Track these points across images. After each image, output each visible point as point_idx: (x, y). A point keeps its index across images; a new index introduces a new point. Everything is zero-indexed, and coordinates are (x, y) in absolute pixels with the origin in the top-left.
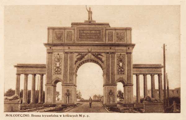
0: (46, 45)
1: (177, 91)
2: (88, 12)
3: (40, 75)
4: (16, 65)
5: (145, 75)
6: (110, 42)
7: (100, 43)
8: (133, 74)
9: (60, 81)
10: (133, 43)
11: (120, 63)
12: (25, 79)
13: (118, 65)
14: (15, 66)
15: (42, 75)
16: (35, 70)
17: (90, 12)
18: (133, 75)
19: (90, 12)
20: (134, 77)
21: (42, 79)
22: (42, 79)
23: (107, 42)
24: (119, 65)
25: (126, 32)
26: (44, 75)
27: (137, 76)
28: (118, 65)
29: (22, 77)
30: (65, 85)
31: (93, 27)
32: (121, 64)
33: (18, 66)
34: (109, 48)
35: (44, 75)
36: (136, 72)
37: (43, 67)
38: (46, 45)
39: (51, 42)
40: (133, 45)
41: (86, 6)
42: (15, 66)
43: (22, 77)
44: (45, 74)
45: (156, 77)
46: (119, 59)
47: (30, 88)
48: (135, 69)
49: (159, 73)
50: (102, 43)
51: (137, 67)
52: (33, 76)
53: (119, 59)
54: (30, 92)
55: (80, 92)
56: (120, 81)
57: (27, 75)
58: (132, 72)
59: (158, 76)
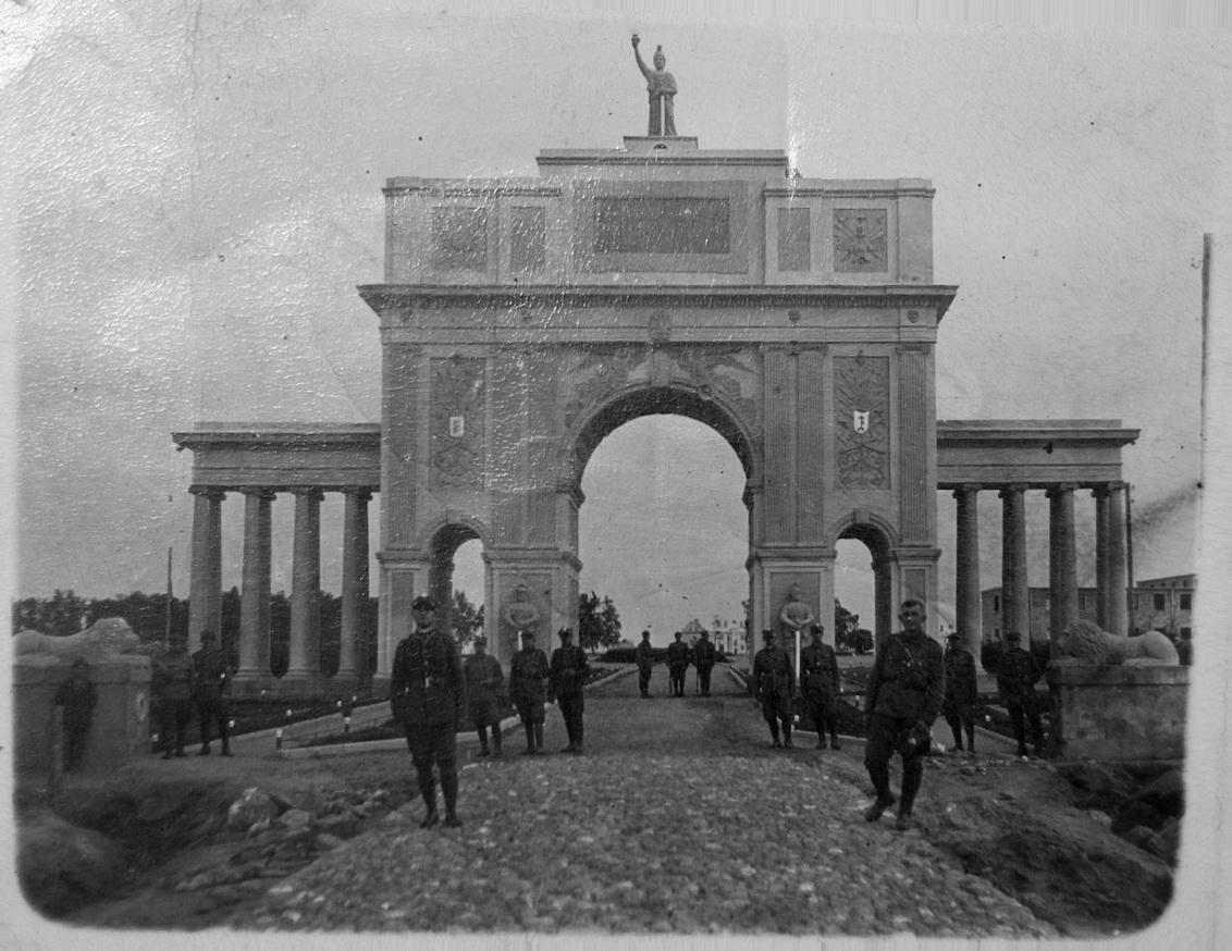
0: (375, 297)
1: (1185, 584)
2: (644, 83)
5: (263, 497)
7: (728, 280)
8: (942, 486)
9: (477, 537)
11: (857, 414)
12: (971, 447)
13: (844, 424)
14: (184, 441)
15: (361, 497)
16: (313, 467)
17: (660, 91)
18: (941, 492)
19: (660, 91)
23: (776, 277)
24: (845, 425)
27: (963, 495)
28: (844, 424)
30: (441, 764)
31: (600, 336)
32: (861, 421)
33: (209, 445)
34: (783, 316)
36: (952, 477)
37: (365, 442)
38: (375, 297)
39: (412, 273)
41: (635, 41)
42: (184, 441)
43: (234, 507)
44: (377, 489)
47: (281, 579)
48: (951, 455)
50: (738, 280)
51: (956, 438)
58: (932, 479)
59: (954, 496)
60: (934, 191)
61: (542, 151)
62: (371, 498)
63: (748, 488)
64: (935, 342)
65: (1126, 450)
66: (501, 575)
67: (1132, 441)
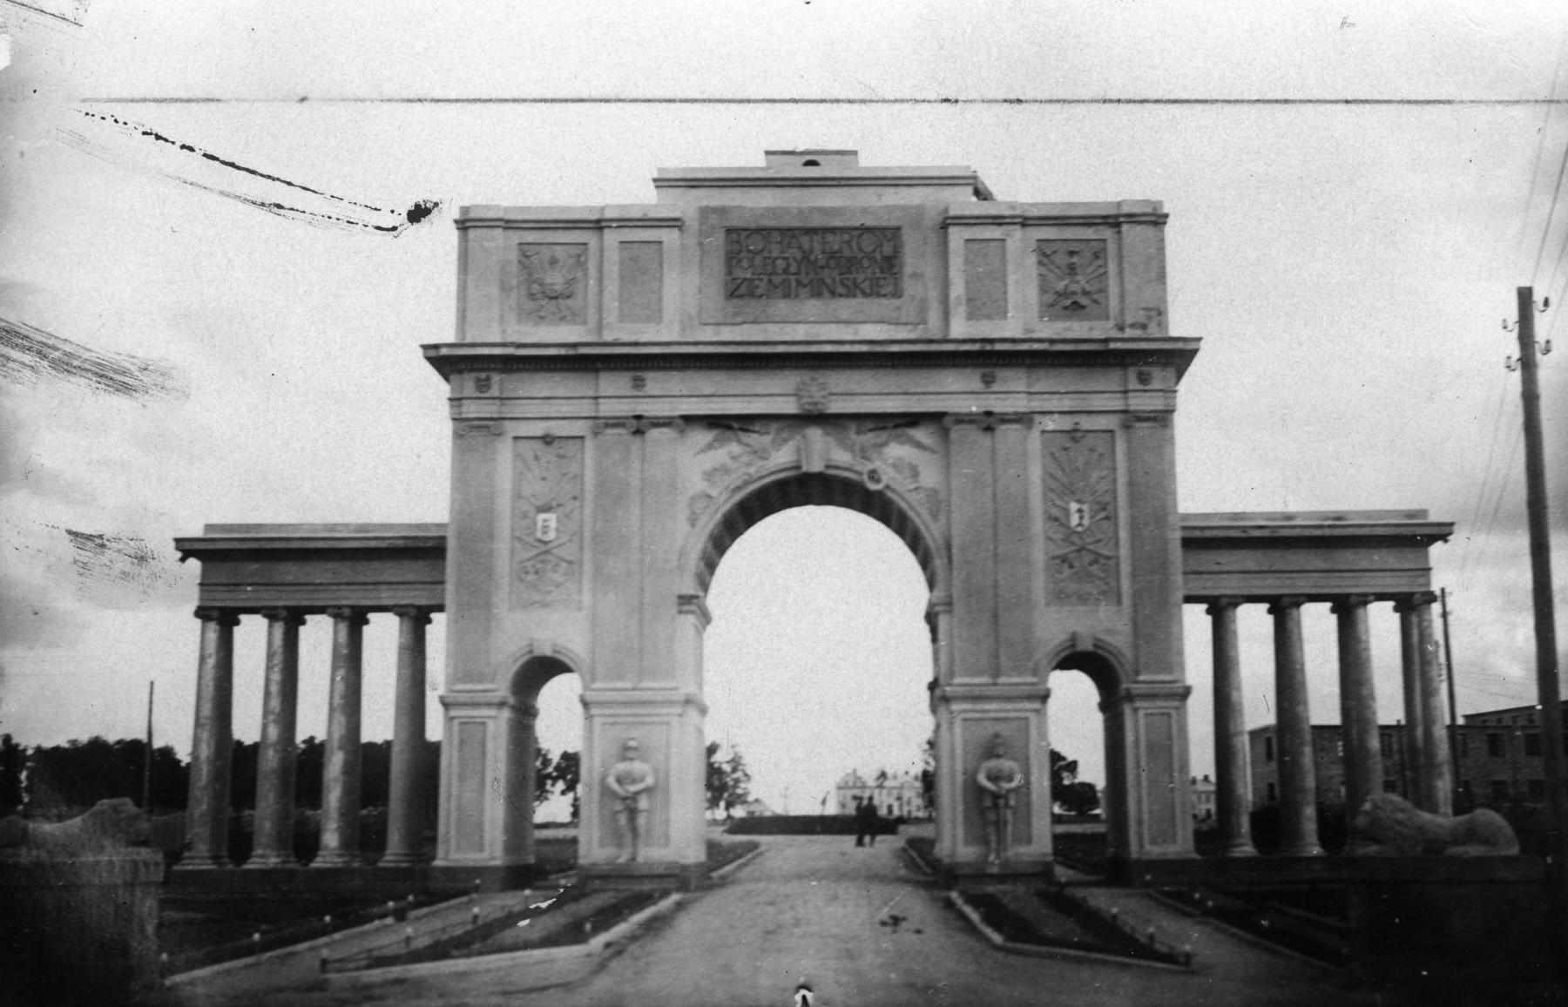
3: (400, 615)
4: (195, 530)
6: (1076, 329)
8: (1189, 599)
9: (565, 669)
10: (1179, 325)
20: (1195, 623)
21: (350, 659)
22: (350, 659)
25: (601, 241)
26: (433, 616)
27: (1220, 610)
29: (253, 635)
35: (433, 616)
38: (446, 362)
40: (1179, 357)
43: (253, 635)
45: (1382, 622)
46: (1059, 474)
49: (1401, 585)
52: (408, 624)
53: (1059, 474)
54: (315, 751)
55: (742, 750)
56: (1065, 664)
57: (355, 620)
60: (1166, 216)
61: (660, 170)
62: (430, 621)
63: (931, 605)
64: (1173, 411)
65: (1436, 550)
66: (1147, 715)
67: (1444, 538)
